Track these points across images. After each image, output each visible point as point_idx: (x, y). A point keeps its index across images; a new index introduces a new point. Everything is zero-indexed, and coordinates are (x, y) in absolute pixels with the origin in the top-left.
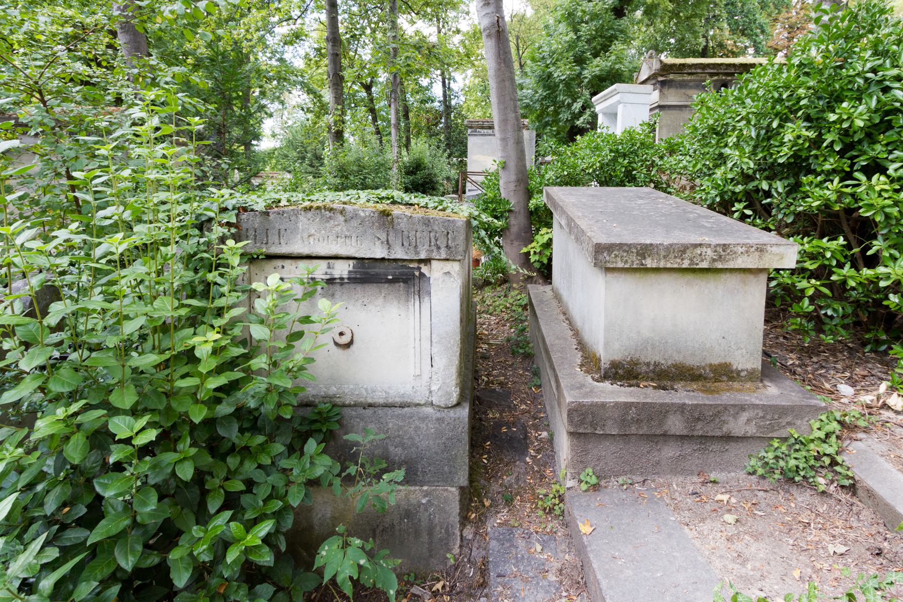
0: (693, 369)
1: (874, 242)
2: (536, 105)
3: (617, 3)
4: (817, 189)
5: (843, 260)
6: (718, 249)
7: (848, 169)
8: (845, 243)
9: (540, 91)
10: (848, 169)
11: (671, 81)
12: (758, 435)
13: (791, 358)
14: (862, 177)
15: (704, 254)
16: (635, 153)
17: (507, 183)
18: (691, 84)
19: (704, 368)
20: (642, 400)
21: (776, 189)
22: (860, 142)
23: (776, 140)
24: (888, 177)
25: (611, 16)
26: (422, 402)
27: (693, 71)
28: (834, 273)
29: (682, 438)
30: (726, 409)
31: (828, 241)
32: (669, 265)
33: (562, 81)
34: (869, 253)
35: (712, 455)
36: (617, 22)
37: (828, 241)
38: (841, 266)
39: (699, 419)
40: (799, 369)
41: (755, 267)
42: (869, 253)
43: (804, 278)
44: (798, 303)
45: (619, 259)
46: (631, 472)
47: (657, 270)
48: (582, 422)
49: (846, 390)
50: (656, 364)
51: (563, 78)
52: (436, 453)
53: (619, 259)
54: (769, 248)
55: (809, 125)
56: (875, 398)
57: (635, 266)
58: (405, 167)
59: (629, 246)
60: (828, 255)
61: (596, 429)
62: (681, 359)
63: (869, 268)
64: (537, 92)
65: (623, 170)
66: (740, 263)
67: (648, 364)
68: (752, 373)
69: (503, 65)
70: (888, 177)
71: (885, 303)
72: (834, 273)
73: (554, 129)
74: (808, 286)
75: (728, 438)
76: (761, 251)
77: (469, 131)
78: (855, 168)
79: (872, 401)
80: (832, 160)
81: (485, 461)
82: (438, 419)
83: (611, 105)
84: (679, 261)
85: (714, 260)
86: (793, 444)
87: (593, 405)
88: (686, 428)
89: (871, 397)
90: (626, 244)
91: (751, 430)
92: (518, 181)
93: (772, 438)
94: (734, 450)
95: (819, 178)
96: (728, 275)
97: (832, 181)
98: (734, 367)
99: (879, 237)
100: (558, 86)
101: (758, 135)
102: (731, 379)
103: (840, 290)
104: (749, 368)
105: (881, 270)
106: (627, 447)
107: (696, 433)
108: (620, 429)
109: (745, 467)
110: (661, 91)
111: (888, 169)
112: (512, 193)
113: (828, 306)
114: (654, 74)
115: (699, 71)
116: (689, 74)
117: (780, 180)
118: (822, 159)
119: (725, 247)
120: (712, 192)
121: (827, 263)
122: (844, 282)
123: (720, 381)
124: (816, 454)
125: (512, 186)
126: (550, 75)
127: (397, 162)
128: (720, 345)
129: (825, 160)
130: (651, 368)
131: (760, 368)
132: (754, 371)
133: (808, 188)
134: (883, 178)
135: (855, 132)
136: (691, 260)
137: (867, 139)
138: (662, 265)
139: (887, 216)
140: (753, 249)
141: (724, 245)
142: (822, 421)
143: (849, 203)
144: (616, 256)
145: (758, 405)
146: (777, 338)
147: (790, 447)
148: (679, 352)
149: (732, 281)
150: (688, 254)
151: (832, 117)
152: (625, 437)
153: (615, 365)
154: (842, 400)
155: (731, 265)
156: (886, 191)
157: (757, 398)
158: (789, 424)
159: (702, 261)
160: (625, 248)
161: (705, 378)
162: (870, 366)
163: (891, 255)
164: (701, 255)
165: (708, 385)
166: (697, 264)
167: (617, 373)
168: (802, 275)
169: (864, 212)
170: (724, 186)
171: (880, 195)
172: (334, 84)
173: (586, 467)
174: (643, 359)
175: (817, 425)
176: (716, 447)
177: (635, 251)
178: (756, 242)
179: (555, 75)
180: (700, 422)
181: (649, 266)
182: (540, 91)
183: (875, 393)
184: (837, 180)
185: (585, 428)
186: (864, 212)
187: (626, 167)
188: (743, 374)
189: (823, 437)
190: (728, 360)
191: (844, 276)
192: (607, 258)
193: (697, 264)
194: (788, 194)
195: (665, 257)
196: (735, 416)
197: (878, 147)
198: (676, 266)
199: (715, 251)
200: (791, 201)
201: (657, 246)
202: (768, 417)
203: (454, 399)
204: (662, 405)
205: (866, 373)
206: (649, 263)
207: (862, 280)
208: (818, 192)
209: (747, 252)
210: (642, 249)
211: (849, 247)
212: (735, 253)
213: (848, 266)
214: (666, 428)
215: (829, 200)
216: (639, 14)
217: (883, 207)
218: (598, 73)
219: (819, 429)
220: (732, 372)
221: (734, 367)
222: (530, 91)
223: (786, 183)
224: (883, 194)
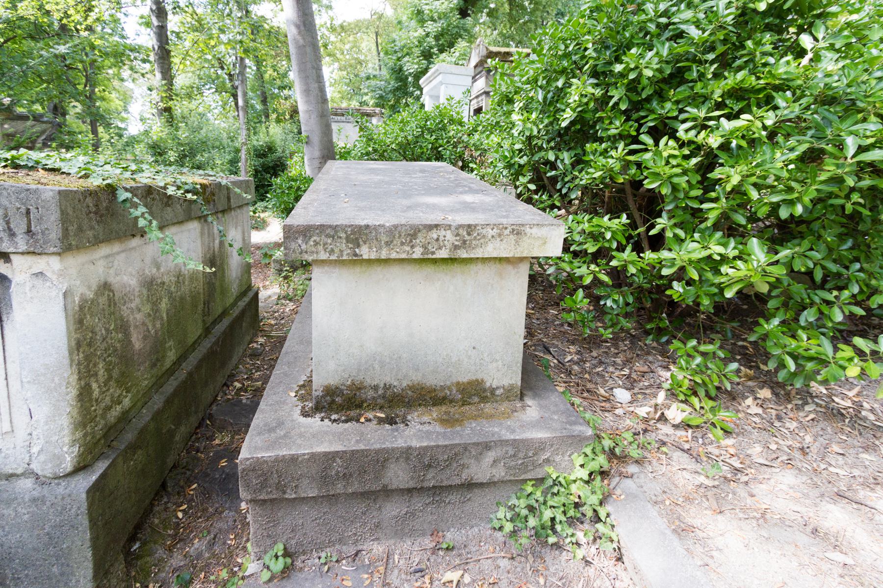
0: (435, 390)
1: (659, 220)
3: (462, 3)
4: (601, 158)
5: (624, 242)
6: (461, 231)
7: (634, 133)
8: (628, 221)
9: (392, 82)
10: (634, 133)
12: (508, 478)
13: (570, 352)
14: (646, 139)
15: (441, 238)
16: (444, 129)
19: (449, 388)
20: (352, 445)
21: (562, 161)
22: (648, 100)
24: (677, 140)
25: (455, 17)
26: (20, 471)
28: (614, 257)
29: (410, 491)
30: (466, 449)
31: (610, 219)
32: (394, 255)
33: (410, 74)
34: (653, 232)
35: (449, 507)
36: (462, 21)
37: (610, 219)
38: (621, 248)
39: (430, 466)
40: (576, 367)
41: (510, 255)
42: (653, 232)
43: (584, 262)
44: (572, 295)
45: (320, 248)
46: (341, 541)
47: (387, 261)
48: (264, 485)
49: (622, 395)
50: (387, 387)
51: (411, 71)
52: (34, 549)
53: (320, 248)
54: (528, 230)
55: (596, 81)
56: (652, 410)
57: (345, 258)
59: (335, 228)
60: (608, 235)
61: (285, 493)
62: (420, 379)
63: (653, 251)
64: (389, 84)
65: (430, 146)
66: (491, 250)
67: (375, 388)
68: (509, 391)
70: (677, 140)
71: (668, 292)
72: (614, 257)
74: (585, 272)
75: (470, 486)
76: (518, 234)
78: (641, 131)
79: (648, 413)
80: (618, 123)
81: (180, 515)
82: (34, 500)
84: (408, 248)
85: (456, 247)
86: (551, 487)
87: (278, 460)
88: (412, 478)
89: (647, 409)
90: (330, 226)
91: (500, 473)
93: (525, 481)
94: (478, 498)
95: (604, 145)
96: (480, 266)
97: (617, 148)
98: (488, 385)
99: (664, 214)
101: (545, 98)
102: (484, 399)
103: (619, 277)
104: (506, 384)
105: (665, 254)
106: (334, 509)
107: (426, 484)
108: (320, 489)
109: (491, 520)
111: (677, 131)
113: (608, 296)
117: (568, 151)
118: (607, 122)
119: (470, 228)
120: (499, 165)
121: (607, 245)
122: (625, 268)
123: (469, 404)
124: (577, 500)
126: (401, 69)
127: (246, 144)
128: (469, 357)
129: (611, 123)
130: (380, 392)
131: (519, 383)
132: (511, 388)
133: (592, 157)
134: (672, 143)
135: (643, 89)
136: (425, 247)
137: (656, 97)
138: (384, 255)
139: (675, 188)
140: (507, 232)
141: (469, 226)
142: (586, 455)
143: (635, 174)
144: (316, 244)
145: (507, 441)
146: (562, 325)
147: (545, 493)
148: (417, 370)
149: (485, 273)
150: (420, 239)
151: (618, 68)
152: (332, 499)
153: (330, 391)
154: (617, 412)
155: (479, 253)
156: (675, 157)
157: (509, 428)
158: (547, 461)
159: (440, 248)
160: (329, 231)
161: (451, 401)
162: (650, 358)
163: (675, 235)
164: (437, 240)
165: (452, 410)
166: (433, 253)
167: (333, 401)
168: (584, 259)
169: (648, 183)
170: (511, 158)
171: (668, 163)
172: (160, 58)
173: (275, 543)
174: (369, 381)
175: (580, 460)
176: (454, 497)
177: (343, 235)
178: (512, 220)
179: (405, 69)
180: (431, 470)
181: (365, 257)
182: (392, 82)
183: (653, 402)
184: (621, 146)
185: (268, 493)
186: (648, 183)
188: (498, 392)
189: (586, 478)
190: (479, 377)
191: (625, 261)
192: (304, 247)
193: (433, 253)
194: (573, 165)
195: (387, 244)
196: (478, 458)
197: (668, 105)
198: (404, 256)
199: (458, 235)
200: (577, 173)
201: (376, 228)
202: (521, 455)
203: (68, 464)
204: (378, 452)
205: (645, 369)
206: (365, 252)
207: (644, 266)
208: (602, 161)
209: (500, 235)
210: (353, 232)
211: (633, 225)
212: (484, 236)
213: (629, 248)
214: (385, 481)
215: (611, 170)
216: (484, 18)
217: (671, 177)
219: (582, 466)
220: (485, 390)
221: (488, 385)
222: (383, 83)
223: (573, 153)
224: (671, 160)
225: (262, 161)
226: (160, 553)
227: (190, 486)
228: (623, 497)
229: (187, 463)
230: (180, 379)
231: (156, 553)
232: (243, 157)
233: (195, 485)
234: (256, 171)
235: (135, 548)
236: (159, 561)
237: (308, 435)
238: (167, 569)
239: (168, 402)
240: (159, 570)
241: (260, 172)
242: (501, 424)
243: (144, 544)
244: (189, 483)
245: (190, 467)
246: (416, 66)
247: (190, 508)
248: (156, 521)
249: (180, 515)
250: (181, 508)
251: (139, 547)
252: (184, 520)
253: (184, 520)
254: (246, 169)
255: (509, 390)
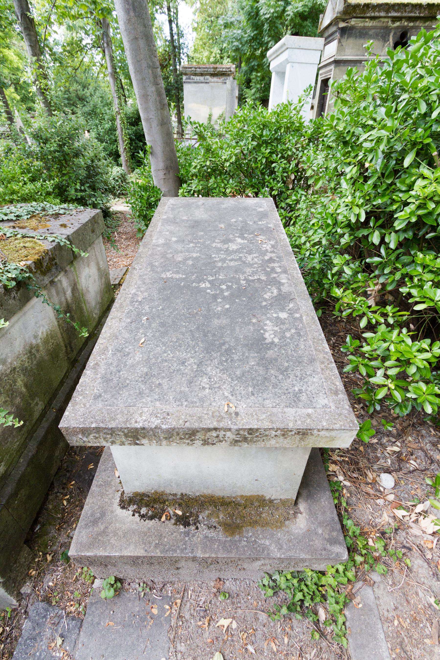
2: (245, 48)
9: (248, 31)
11: (352, 28)
17: (157, 170)
18: (371, 32)
23: (403, 182)
27: (377, 14)
33: (267, 19)
58: (128, 118)
69: (132, 14)
73: (259, 74)
77: (184, 78)
79: (403, 517)
81: (65, 503)
83: (281, 64)
92: (167, 168)
98: (267, 498)
100: (263, 25)
110: (339, 42)
112: (162, 182)
114: (336, 18)
115: (382, 14)
116: (373, 18)
125: (161, 174)
127: (119, 114)
174: (168, 491)
187: (267, 158)
218: (300, 9)
221: (267, 498)
225: (135, 128)
226: (53, 532)
227: (70, 483)
228: (360, 606)
229: (67, 466)
230: (50, 420)
231: (50, 533)
232: (119, 126)
233: (73, 482)
234: (130, 139)
235: (37, 529)
236: (52, 538)
237: (120, 533)
238: (57, 544)
239: (41, 444)
240: (53, 544)
241: (134, 140)
242: (272, 535)
243: (43, 525)
244: (69, 480)
245: (70, 469)
246: (272, 11)
247: (71, 497)
248: (51, 507)
249: (65, 503)
250: (66, 498)
251: (40, 529)
252: (68, 507)
253: (68, 507)
254: (122, 139)
255: (284, 502)
